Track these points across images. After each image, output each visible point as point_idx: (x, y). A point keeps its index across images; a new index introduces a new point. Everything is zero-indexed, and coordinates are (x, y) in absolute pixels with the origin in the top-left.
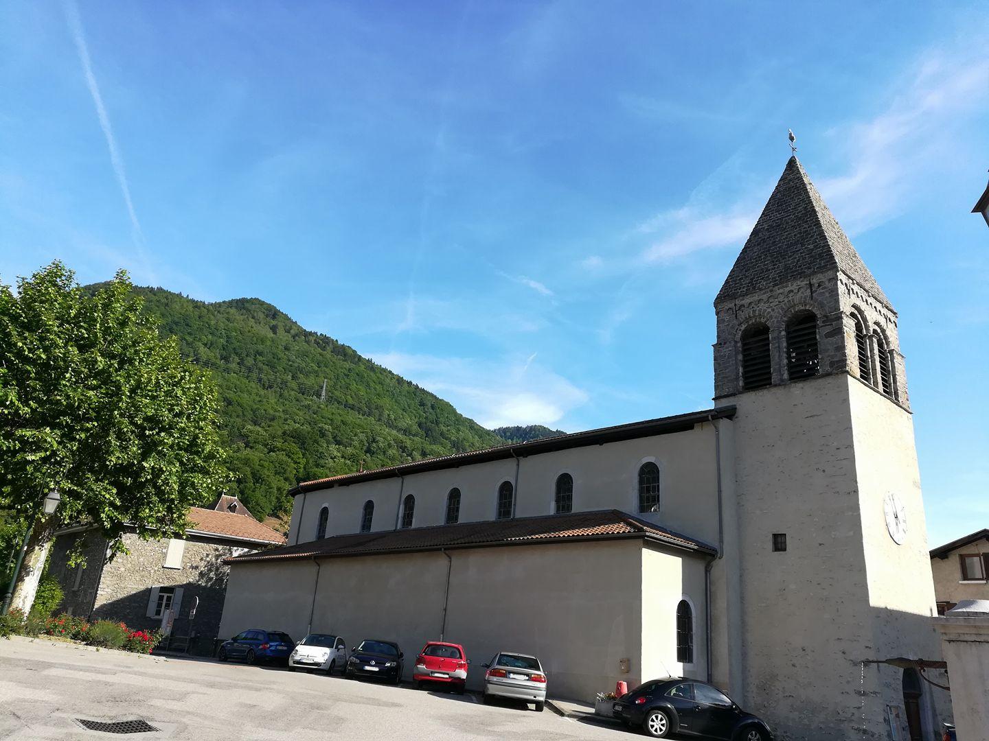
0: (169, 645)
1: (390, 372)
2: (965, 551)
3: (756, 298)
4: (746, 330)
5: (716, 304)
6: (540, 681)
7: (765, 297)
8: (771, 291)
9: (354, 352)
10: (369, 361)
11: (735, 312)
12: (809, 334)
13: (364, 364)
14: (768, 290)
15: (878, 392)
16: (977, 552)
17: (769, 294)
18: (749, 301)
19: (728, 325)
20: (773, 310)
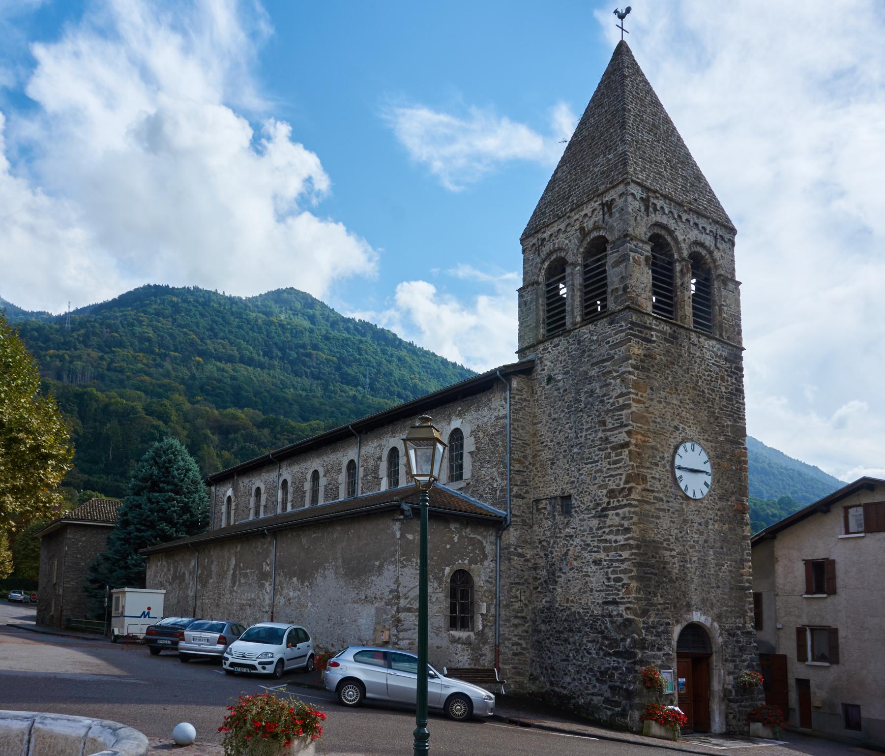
0: (515, 460)
1: (433, 354)
2: (847, 502)
3: (556, 229)
4: (549, 267)
5: (522, 241)
6: (282, 509)
7: (562, 226)
8: (569, 217)
9: (395, 335)
10: (411, 344)
11: (537, 248)
12: (598, 267)
13: (406, 348)
14: (566, 217)
15: (808, 626)
16: (858, 503)
17: (566, 223)
18: (549, 233)
19: (532, 264)
20: (570, 241)
